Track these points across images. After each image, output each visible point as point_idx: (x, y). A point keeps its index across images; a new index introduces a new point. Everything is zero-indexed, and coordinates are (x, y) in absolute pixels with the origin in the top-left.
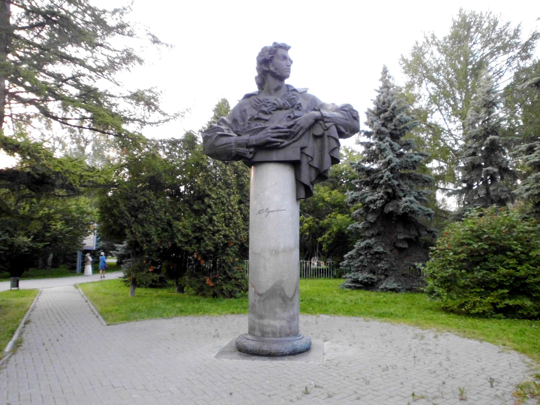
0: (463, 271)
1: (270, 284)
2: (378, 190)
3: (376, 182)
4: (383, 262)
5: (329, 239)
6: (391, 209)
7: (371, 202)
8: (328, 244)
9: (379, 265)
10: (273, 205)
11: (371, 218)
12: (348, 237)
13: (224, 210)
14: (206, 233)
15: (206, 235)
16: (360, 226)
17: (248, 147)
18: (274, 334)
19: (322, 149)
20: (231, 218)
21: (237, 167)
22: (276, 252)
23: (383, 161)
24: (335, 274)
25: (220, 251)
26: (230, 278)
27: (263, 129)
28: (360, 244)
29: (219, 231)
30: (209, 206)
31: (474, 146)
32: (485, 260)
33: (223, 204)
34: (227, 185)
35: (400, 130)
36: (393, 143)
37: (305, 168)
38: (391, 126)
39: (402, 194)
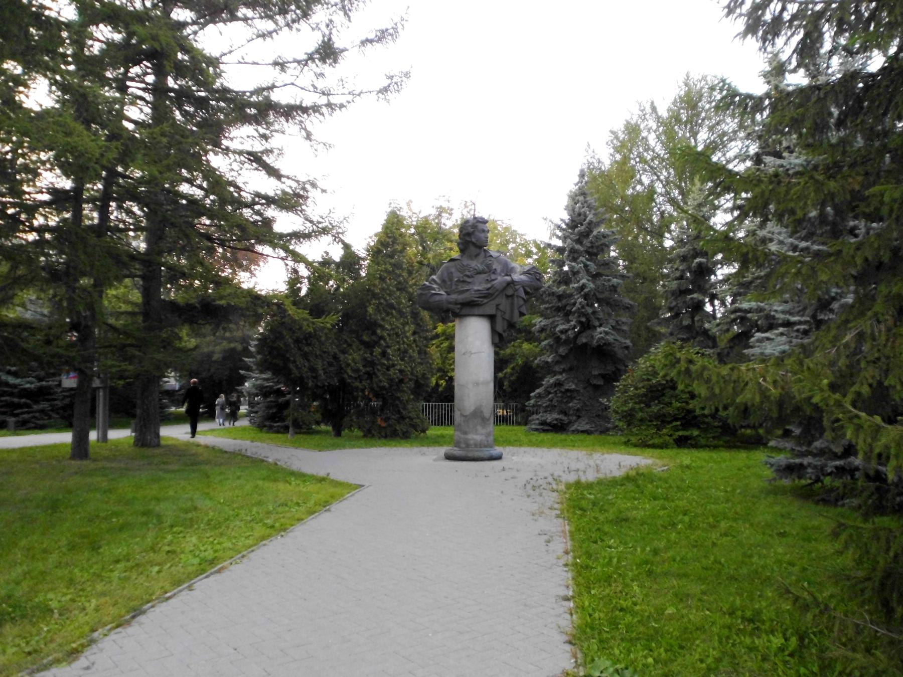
0: (643, 405)
1: (473, 408)
2: (571, 317)
3: (568, 308)
4: (575, 401)
5: (512, 374)
6: (584, 340)
7: (562, 332)
8: (510, 381)
9: (571, 404)
10: (474, 349)
11: (562, 350)
12: (538, 372)
13: (398, 342)
14: (379, 367)
15: (378, 370)
16: (549, 360)
17: (456, 304)
18: (476, 445)
19: (512, 304)
20: (406, 351)
21: (412, 294)
22: (477, 384)
23: (576, 285)
24: (520, 420)
25: (395, 387)
26: (403, 418)
27: (468, 290)
28: (549, 380)
29: (394, 365)
30: (382, 338)
31: (681, 268)
32: (663, 395)
33: (397, 335)
34: (402, 314)
35: (597, 247)
36: (588, 263)
37: (499, 320)
38: (586, 242)
39: (597, 323)
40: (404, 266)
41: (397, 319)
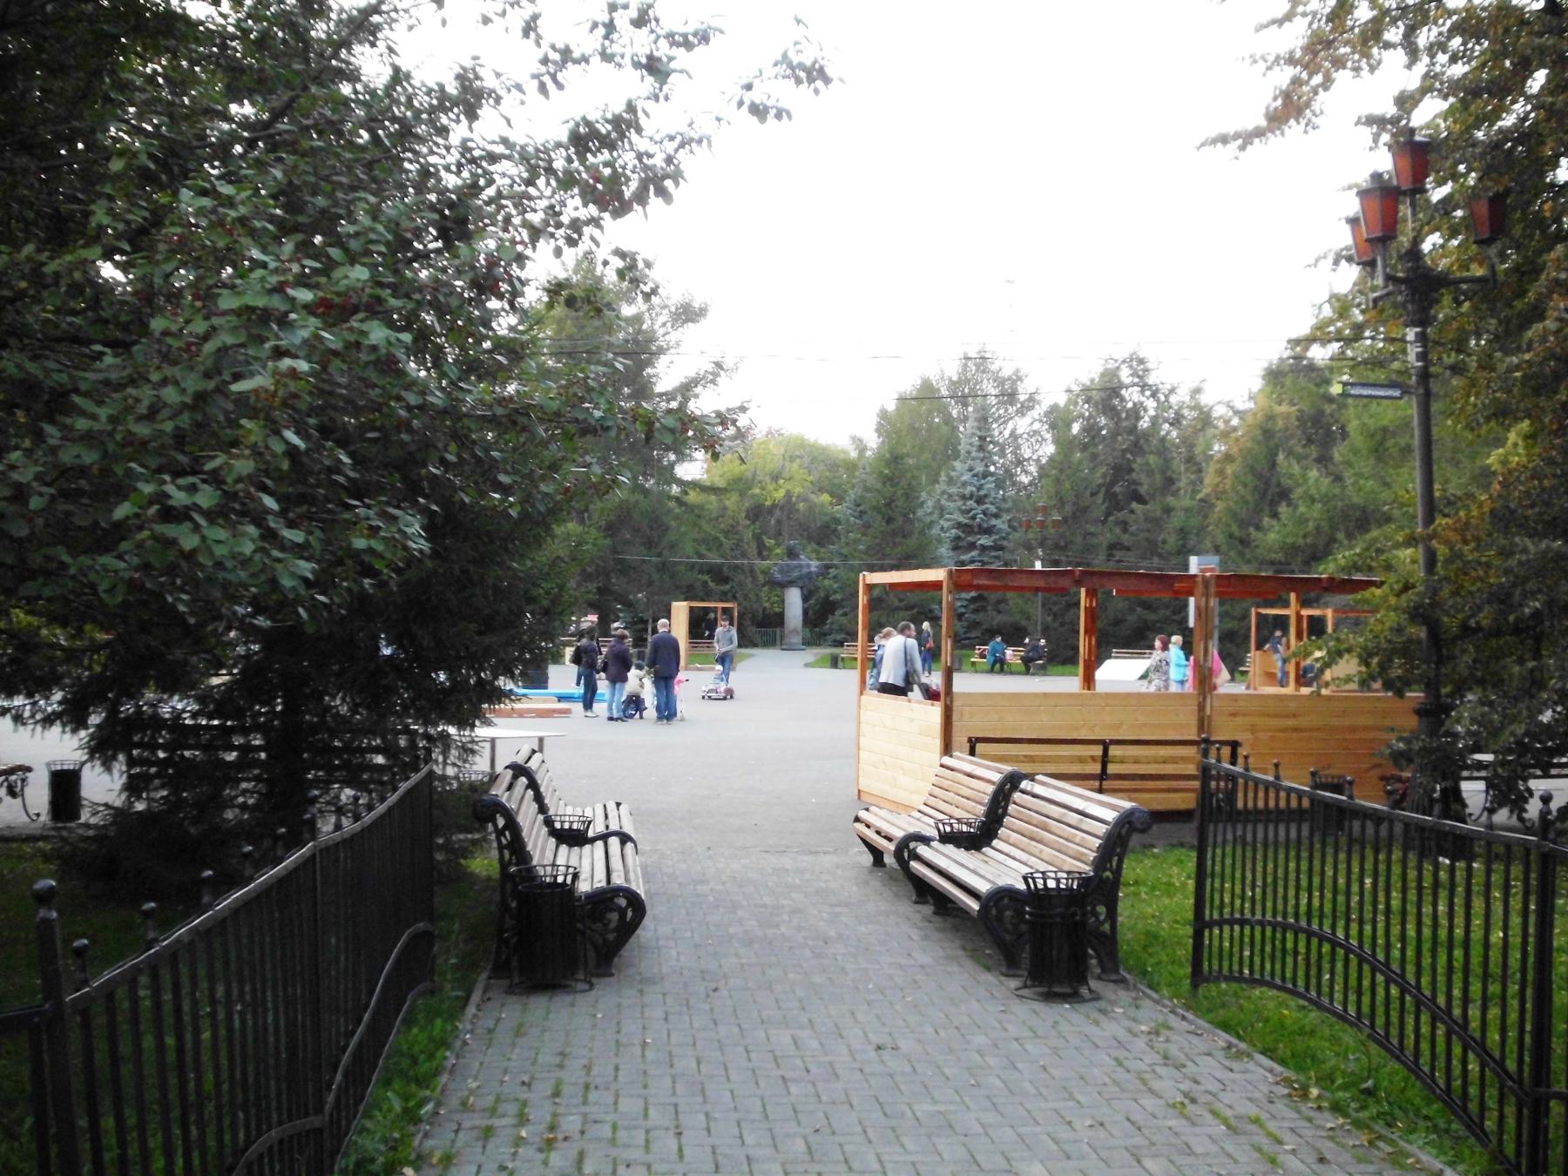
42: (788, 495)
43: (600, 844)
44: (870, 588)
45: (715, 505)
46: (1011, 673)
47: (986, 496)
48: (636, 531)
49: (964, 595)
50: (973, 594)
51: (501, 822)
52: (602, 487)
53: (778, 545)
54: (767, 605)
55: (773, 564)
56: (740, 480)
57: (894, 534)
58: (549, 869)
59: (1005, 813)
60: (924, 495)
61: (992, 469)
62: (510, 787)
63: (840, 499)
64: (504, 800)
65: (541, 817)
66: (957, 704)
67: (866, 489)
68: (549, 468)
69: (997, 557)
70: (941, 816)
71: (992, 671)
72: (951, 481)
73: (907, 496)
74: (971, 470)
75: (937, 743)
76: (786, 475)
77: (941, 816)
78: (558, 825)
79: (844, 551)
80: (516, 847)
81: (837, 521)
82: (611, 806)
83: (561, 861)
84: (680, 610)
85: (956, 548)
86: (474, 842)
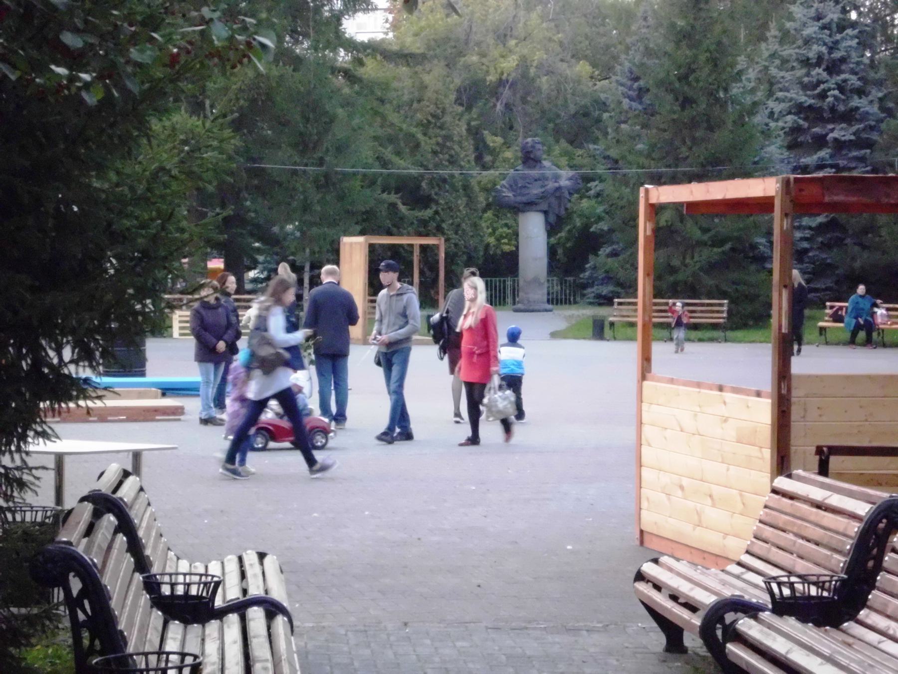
5: (568, 239)
13: (452, 216)
20: (459, 225)
33: (450, 208)
40: (455, 139)
41: (451, 194)
42: (524, 63)
43: (233, 618)
44: (656, 210)
45: (408, 83)
46: (884, 345)
47: (843, 60)
48: (282, 123)
49: (806, 221)
50: (821, 219)
51: (76, 585)
52: (232, 55)
53: (507, 145)
54: (492, 240)
55: (503, 174)
56: (447, 40)
57: (693, 124)
58: (153, 659)
59: (879, 567)
60: (742, 61)
61: (854, 15)
62: (90, 531)
63: (607, 71)
64: (80, 549)
65: (139, 578)
66: (797, 394)
67: (648, 52)
68: (143, 24)
69: (862, 159)
70: (775, 572)
71: (852, 341)
72: (785, 37)
73: (714, 63)
74: (818, 18)
75: (766, 455)
76: (520, 30)
77: (775, 572)
78: (166, 590)
79: (613, 153)
80: (103, 625)
81: (603, 106)
82: (251, 558)
83: (171, 645)
84: (355, 248)
85: (792, 146)
86: (30, 620)
